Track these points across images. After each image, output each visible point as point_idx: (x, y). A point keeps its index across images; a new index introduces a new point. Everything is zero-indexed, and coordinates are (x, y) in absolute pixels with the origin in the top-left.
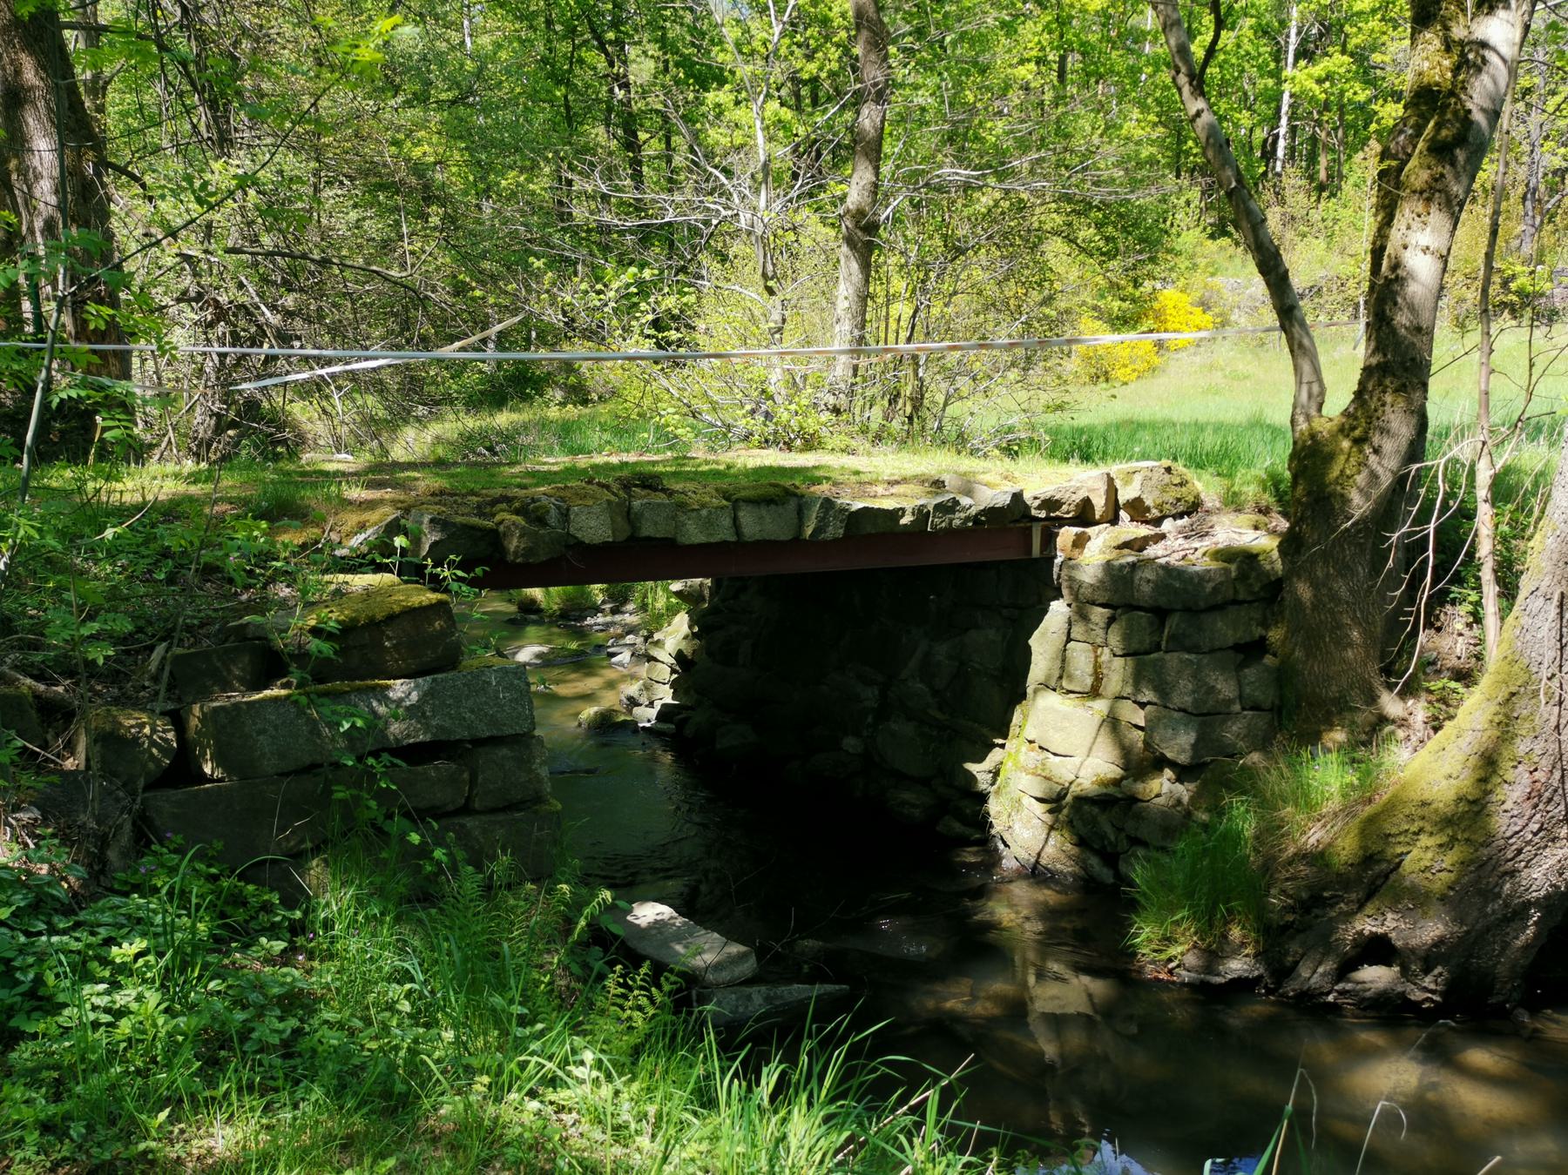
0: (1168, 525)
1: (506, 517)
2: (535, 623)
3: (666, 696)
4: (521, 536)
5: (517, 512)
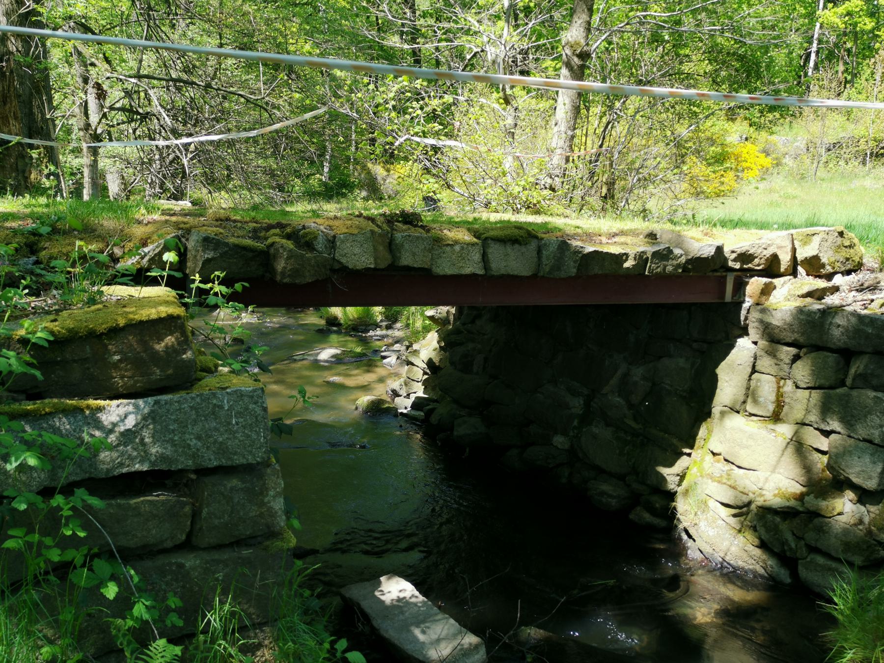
0: (838, 280)
1: (275, 238)
2: (335, 332)
3: (419, 391)
4: (288, 258)
5: (288, 237)
